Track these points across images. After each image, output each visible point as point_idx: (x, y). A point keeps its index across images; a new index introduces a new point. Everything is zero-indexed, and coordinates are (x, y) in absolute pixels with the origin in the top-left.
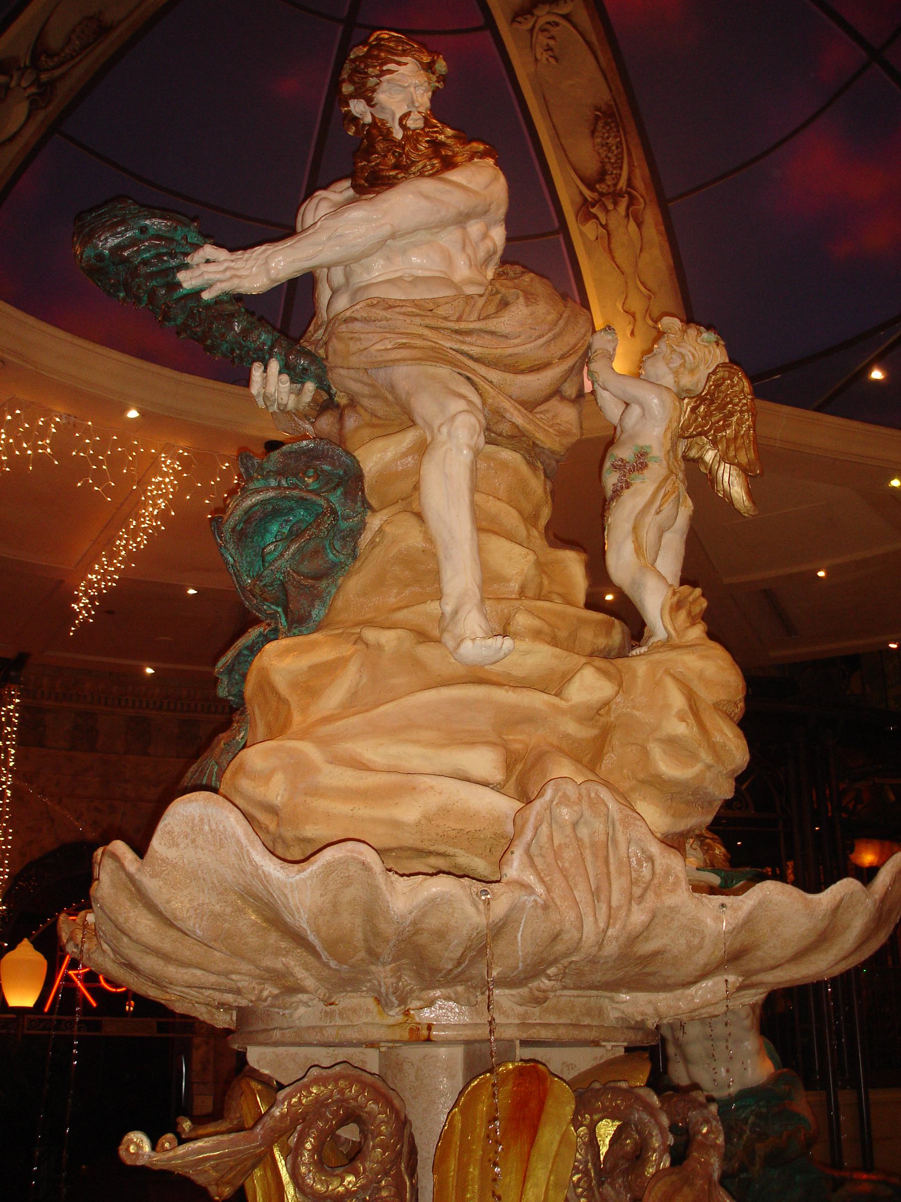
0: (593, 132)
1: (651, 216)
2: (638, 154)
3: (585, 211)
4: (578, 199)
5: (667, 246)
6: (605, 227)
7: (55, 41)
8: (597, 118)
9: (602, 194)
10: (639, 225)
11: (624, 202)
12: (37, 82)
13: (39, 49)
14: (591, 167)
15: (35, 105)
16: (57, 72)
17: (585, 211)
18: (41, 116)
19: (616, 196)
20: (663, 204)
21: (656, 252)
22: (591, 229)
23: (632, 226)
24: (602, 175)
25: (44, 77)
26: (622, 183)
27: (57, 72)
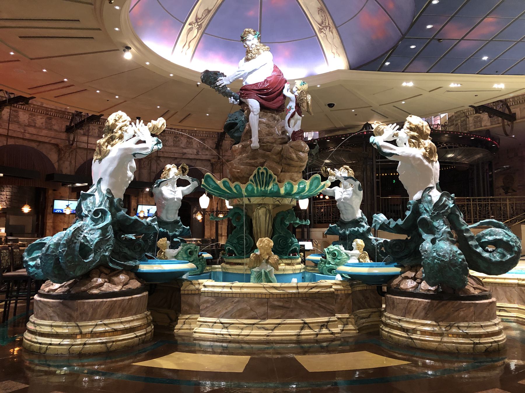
0: (319, 13)
1: (334, 31)
2: (329, 17)
3: (320, 30)
4: (319, 28)
5: (339, 37)
6: (325, 34)
7: (199, 16)
8: (319, 10)
9: (323, 27)
10: (332, 33)
11: (328, 28)
12: (198, 25)
13: (197, 19)
14: (320, 21)
15: (198, 29)
16: (201, 22)
17: (320, 30)
18: (200, 31)
19: (326, 27)
20: (336, 28)
21: (337, 39)
22: (322, 35)
23: (331, 33)
24: (322, 22)
25: (199, 24)
26: (327, 24)
27: (201, 22)
